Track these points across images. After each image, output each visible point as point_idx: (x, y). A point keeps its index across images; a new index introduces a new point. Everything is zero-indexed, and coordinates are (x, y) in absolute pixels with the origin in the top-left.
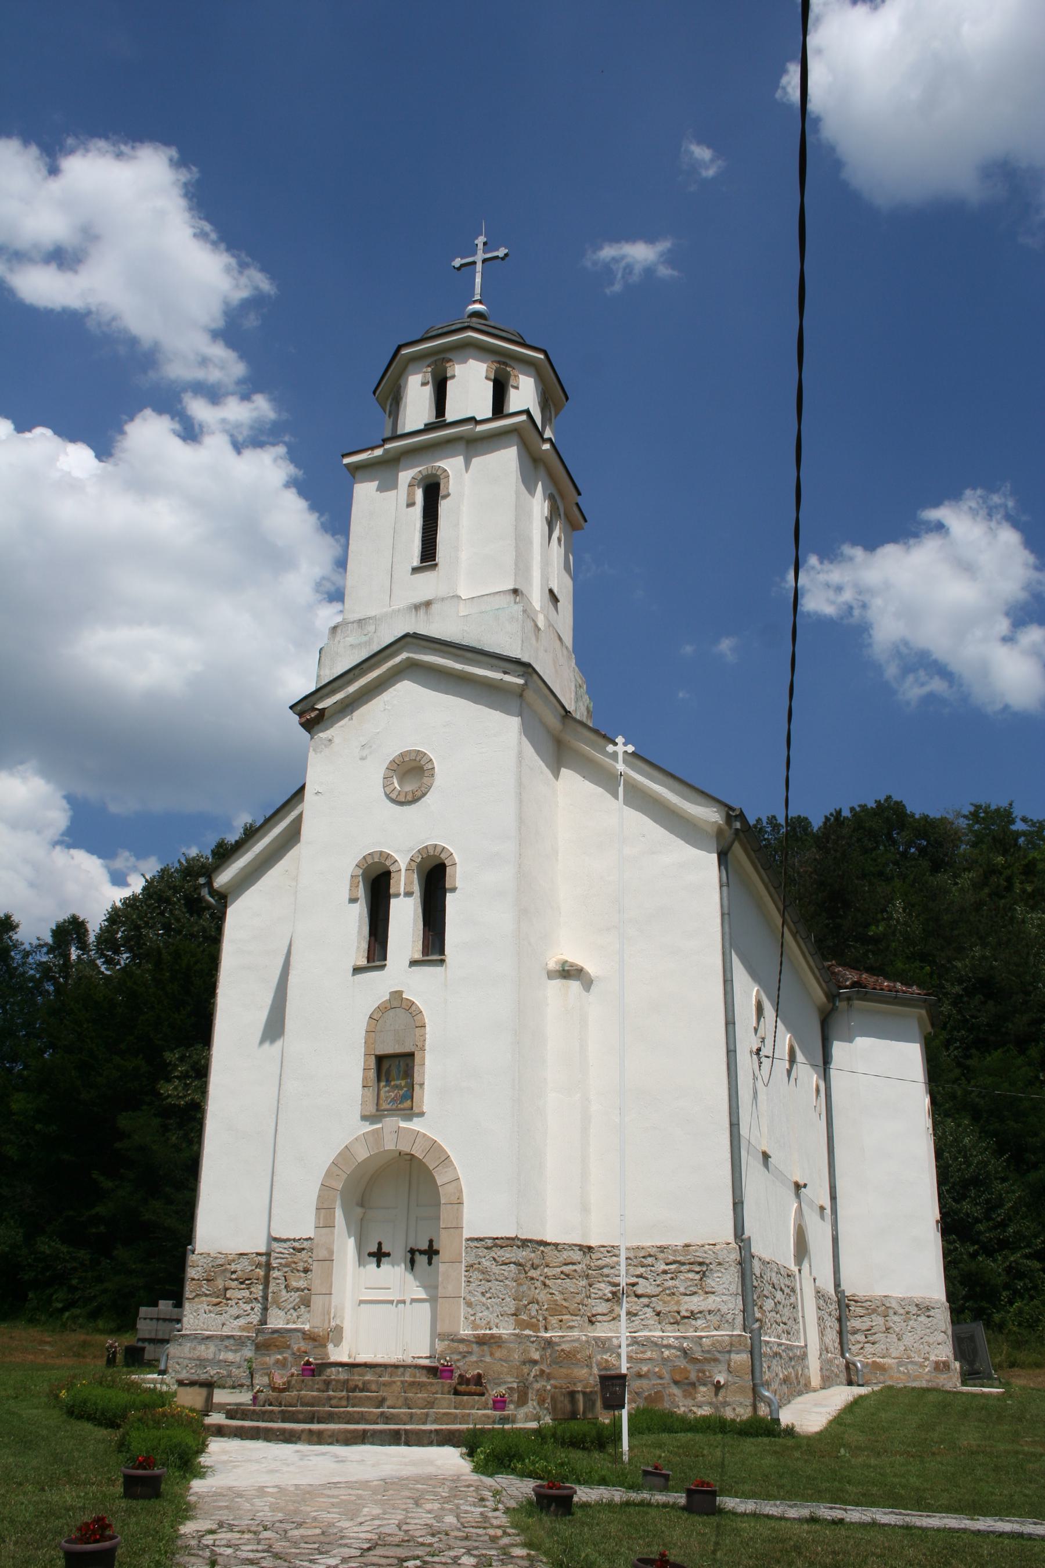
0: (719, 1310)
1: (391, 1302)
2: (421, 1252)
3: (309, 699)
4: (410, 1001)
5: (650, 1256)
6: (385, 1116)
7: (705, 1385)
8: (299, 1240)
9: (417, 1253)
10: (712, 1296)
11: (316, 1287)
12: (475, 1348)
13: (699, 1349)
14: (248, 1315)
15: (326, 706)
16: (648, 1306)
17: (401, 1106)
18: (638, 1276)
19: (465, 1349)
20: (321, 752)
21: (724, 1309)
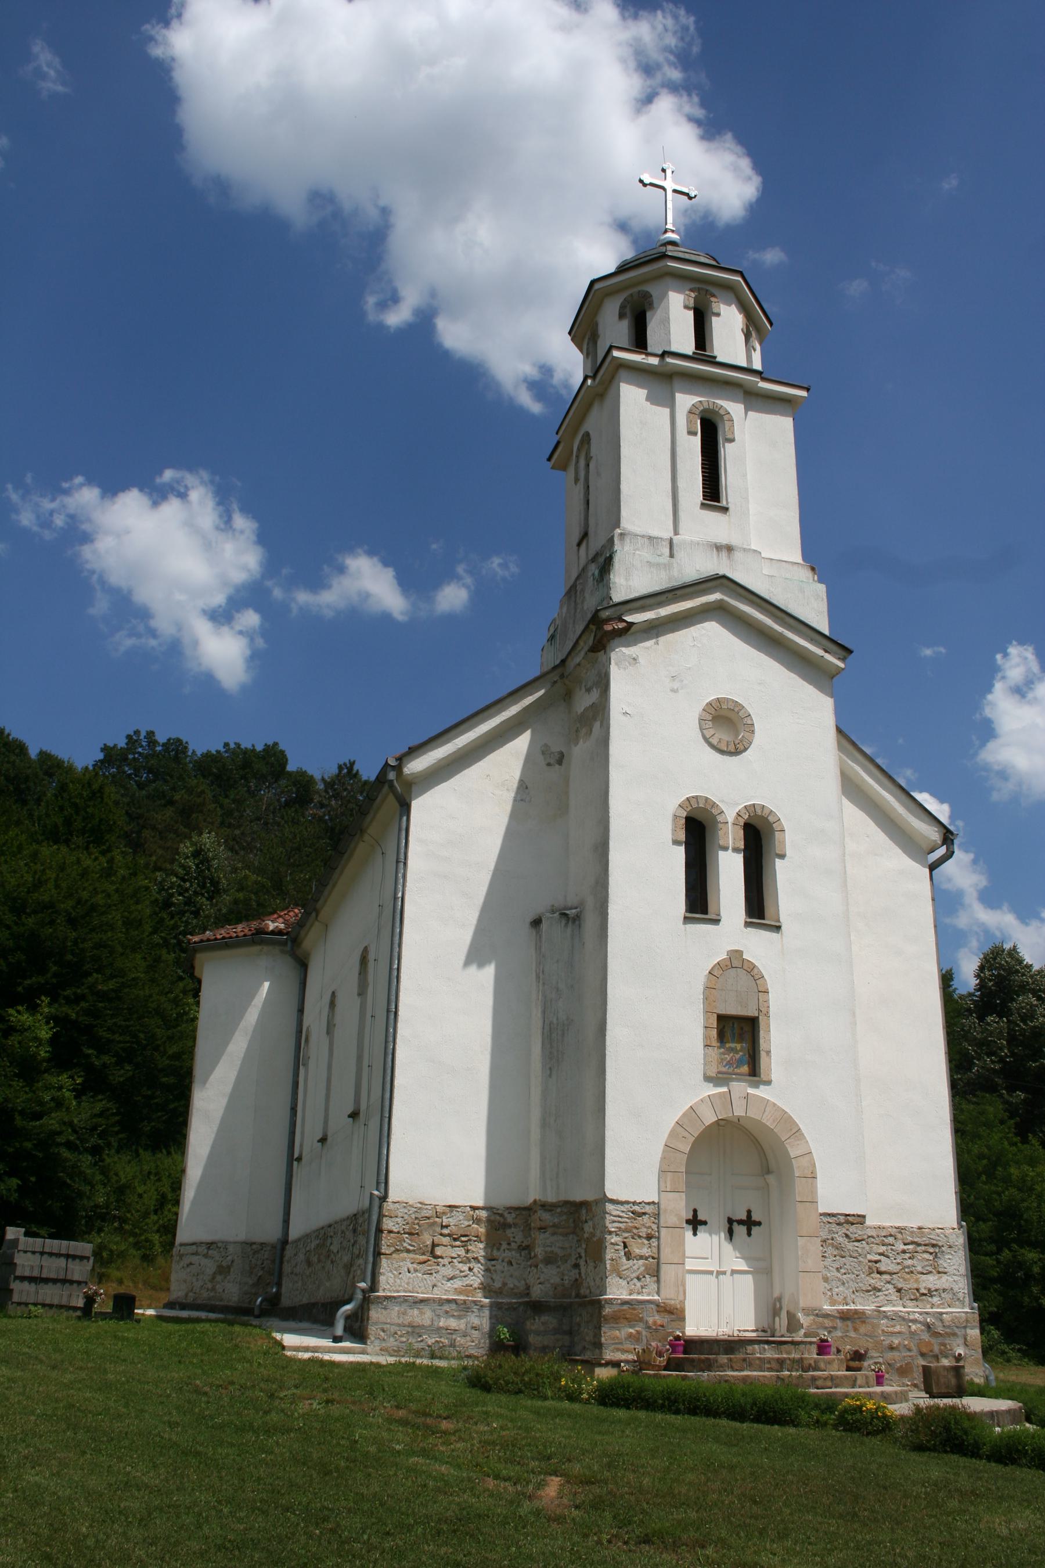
0: (952, 1289)
1: (711, 1273)
2: (740, 1222)
3: (618, 608)
4: (752, 963)
5: (891, 1235)
6: (733, 1080)
7: (946, 1357)
8: (640, 1203)
9: (735, 1224)
10: (945, 1275)
11: (666, 1254)
12: (839, 1323)
13: (940, 1324)
14: (465, 1276)
15: (635, 621)
16: (889, 1282)
17: (737, 1071)
18: (881, 1254)
19: (831, 1325)
20: (625, 669)
21: (956, 1288)
